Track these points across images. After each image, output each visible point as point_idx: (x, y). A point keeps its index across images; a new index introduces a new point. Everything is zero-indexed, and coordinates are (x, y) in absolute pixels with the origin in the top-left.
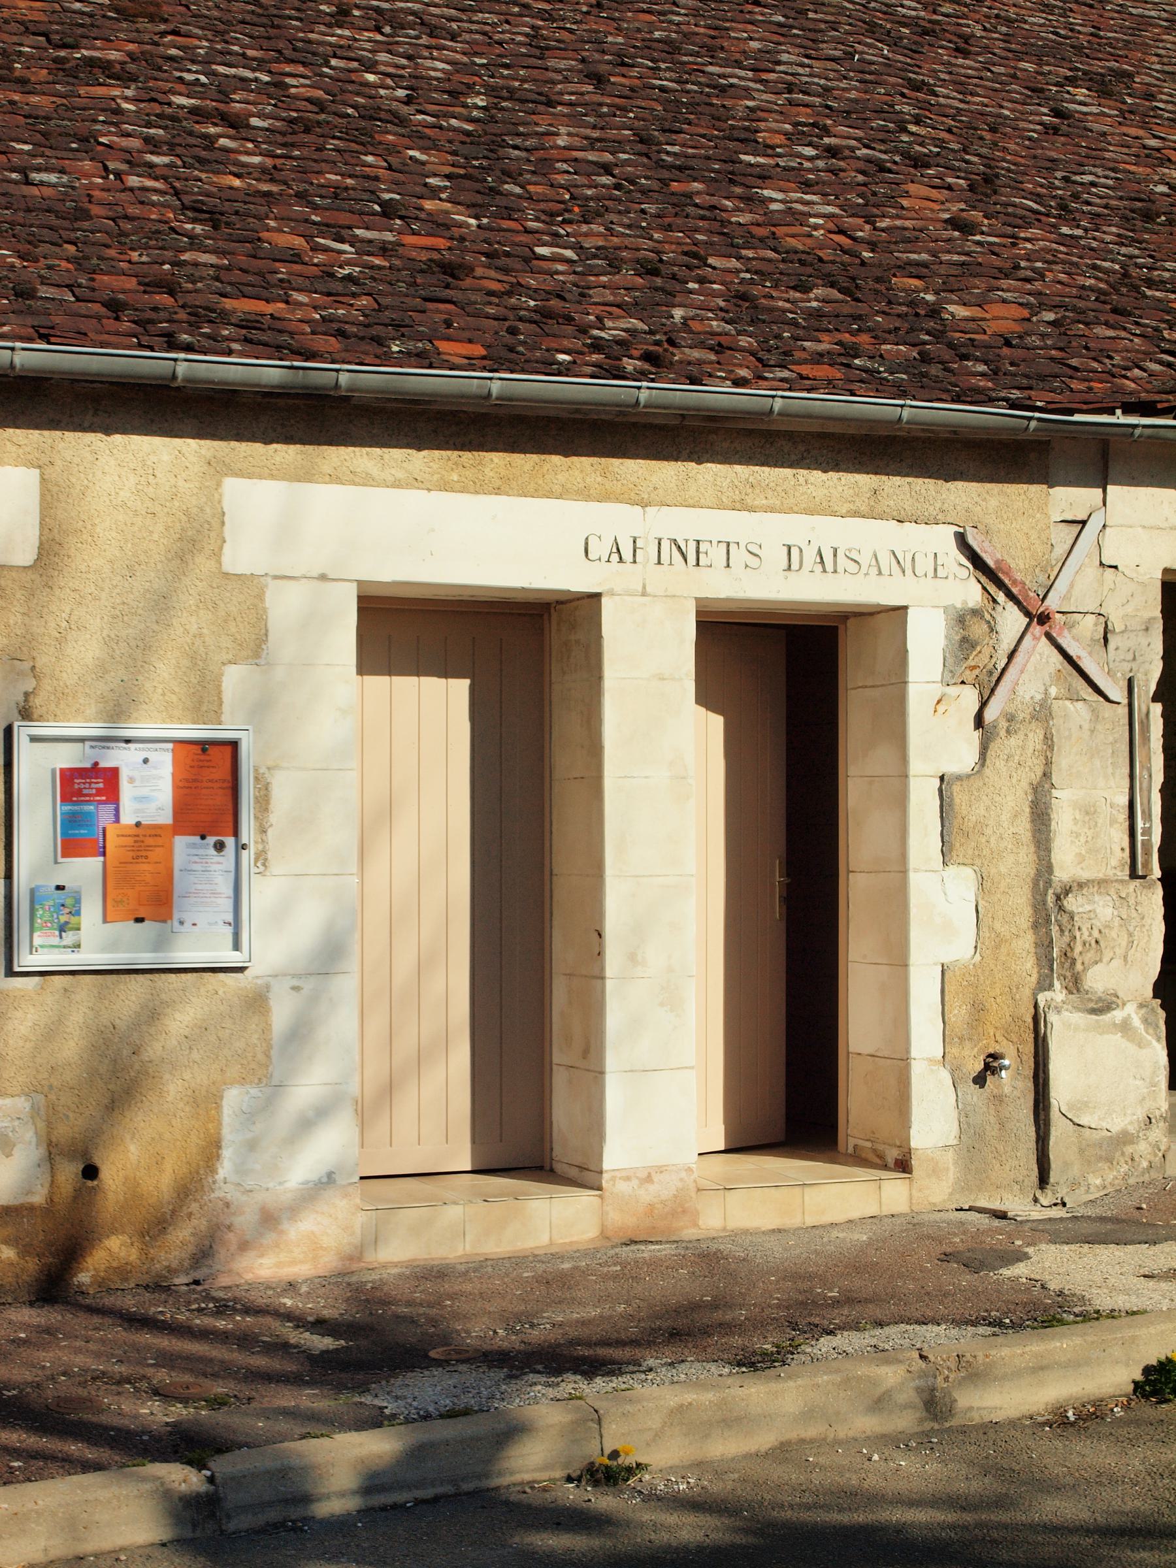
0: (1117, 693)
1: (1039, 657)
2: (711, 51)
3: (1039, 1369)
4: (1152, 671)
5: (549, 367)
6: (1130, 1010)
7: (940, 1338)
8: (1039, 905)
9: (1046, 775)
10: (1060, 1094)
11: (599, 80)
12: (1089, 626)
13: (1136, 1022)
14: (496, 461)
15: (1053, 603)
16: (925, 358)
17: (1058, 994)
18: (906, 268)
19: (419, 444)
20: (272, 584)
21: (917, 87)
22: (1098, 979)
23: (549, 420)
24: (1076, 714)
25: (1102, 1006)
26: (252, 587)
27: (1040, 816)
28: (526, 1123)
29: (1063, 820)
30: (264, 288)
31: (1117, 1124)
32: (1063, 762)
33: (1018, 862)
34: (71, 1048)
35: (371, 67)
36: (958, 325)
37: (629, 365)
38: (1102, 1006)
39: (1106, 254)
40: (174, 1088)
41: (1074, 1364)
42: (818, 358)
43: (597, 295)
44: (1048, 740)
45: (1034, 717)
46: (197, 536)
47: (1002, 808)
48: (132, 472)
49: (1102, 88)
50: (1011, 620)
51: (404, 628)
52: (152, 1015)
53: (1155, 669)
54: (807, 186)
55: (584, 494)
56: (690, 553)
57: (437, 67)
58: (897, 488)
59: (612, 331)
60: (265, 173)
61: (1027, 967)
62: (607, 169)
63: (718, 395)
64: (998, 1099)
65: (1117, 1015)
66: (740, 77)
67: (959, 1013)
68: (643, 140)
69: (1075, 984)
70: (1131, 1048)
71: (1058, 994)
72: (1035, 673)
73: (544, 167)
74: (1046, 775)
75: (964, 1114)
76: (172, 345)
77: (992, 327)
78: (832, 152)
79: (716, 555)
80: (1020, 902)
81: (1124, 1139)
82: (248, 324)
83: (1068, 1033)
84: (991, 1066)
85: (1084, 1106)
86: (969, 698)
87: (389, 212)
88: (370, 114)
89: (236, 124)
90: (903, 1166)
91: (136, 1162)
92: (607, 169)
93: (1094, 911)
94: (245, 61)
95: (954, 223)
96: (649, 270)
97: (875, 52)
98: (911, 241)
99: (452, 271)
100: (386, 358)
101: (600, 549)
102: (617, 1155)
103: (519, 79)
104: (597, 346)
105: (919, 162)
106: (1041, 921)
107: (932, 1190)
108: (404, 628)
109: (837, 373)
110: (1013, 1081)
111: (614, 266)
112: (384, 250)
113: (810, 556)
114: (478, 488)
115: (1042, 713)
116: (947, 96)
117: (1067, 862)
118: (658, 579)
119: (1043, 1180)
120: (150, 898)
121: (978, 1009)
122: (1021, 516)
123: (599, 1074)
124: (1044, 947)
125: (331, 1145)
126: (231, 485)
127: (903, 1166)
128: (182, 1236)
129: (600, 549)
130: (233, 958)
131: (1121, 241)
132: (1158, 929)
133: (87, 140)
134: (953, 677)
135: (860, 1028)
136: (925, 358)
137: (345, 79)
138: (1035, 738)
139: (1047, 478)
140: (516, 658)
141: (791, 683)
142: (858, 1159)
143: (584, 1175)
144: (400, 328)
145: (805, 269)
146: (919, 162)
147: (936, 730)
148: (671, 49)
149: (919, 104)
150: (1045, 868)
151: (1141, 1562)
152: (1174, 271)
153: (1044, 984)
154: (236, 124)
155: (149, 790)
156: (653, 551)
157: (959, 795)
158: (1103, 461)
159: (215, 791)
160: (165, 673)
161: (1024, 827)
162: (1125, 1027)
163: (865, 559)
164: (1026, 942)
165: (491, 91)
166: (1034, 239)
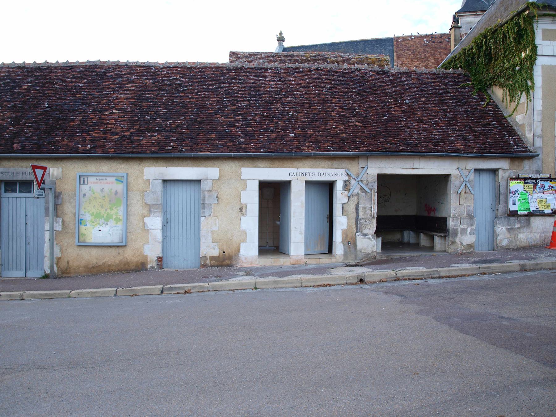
6: (370, 236)
14: (277, 163)
20: (248, 181)
23: (269, 158)
29: (360, 210)
32: (361, 201)
38: (365, 235)
44: (358, 198)
45: (356, 195)
47: (351, 208)
55: (289, 167)
56: (304, 174)
58: (335, 163)
61: (355, 230)
65: (368, 237)
69: (362, 233)
85: (361, 250)
113: (322, 174)
115: (358, 194)
117: (361, 214)
118: (299, 178)
121: (347, 236)
122: (355, 167)
124: (357, 227)
138: (356, 198)
152: (555, 213)
156: (297, 175)
161: (354, 210)
162: (369, 238)
164: (354, 226)
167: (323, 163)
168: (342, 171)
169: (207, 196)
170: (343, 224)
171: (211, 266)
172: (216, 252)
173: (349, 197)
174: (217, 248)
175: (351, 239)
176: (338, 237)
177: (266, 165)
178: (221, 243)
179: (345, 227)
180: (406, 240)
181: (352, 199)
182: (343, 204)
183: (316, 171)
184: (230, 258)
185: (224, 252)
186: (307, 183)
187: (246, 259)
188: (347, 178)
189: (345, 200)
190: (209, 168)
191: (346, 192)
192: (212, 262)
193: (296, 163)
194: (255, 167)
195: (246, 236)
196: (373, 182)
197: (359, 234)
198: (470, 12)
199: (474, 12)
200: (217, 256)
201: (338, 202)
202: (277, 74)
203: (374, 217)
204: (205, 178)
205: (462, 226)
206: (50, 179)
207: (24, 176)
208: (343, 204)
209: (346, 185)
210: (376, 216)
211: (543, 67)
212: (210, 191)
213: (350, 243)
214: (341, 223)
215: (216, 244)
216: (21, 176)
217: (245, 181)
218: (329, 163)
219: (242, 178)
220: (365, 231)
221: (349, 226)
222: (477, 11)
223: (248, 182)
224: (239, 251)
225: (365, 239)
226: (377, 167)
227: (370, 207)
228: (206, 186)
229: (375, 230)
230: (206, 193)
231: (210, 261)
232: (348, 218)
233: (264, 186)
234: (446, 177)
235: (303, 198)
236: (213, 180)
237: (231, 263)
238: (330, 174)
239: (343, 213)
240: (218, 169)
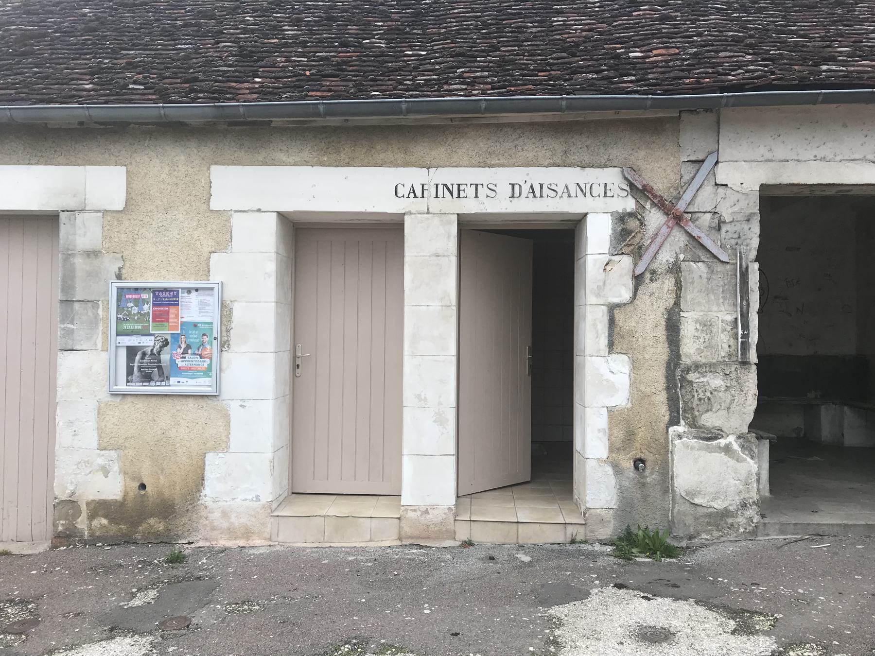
6: (731, 439)
9: (677, 304)
13: (736, 446)
27: (673, 327)
29: (688, 329)
32: (689, 296)
38: (711, 435)
44: (679, 286)
50: (655, 219)
56: (455, 191)
61: (663, 412)
65: (722, 442)
69: (693, 424)
70: (732, 462)
74: (677, 304)
80: (657, 376)
81: (725, 513)
101: (403, 191)
113: (526, 189)
117: (690, 349)
118: (436, 205)
121: (630, 436)
124: (673, 402)
129: (403, 191)
138: (669, 283)
156: (433, 196)
157: (619, 315)
161: (661, 333)
162: (727, 449)
163: (560, 189)
164: (662, 397)
167: (531, 147)
168: (612, 176)
169: (79, 274)
170: (612, 388)
171: (93, 541)
172: (112, 488)
173: (638, 280)
174: (116, 468)
175: (649, 447)
176: (592, 438)
177: (306, 155)
178: (131, 453)
179: (621, 399)
180: (827, 432)
181: (649, 287)
182: (612, 308)
183: (503, 177)
184: (166, 509)
185: (143, 486)
186: (610, 353)
187: (225, 515)
188: (630, 204)
189: (624, 294)
190: (90, 168)
191: (626, 261)
192: (95, 523)
193: (421, 150)
194: (266, 164)
195: (228, 424)
196: (739, 217)
197: (681, 428)
200: (115, 502)
201: (591, 299)
203: (745, 363)
204: (71, 204)
208: (612, 308)
209: (626, 235)
210: (753, 356)
212: (92, 254)
213: (645, 465)
214: (606, 384)
215: (113, 454)
217: (224, 216)
218: (557, 145)
219: (214, 205)
220: (709, 420)
223: (237, 221)
224: (200, 481)
225: (710, 450)
226: (743, 170)
227: (718, 322)
228: (84, 234)
229: (750, 418)
230: (78, 261)
231: (92, 517)
232: (635, 365)
233: (776, 203)
235: (449, 283)
236: (105, 212)
237: (168, 530)
238: (560, 189)
239: (611, 345)
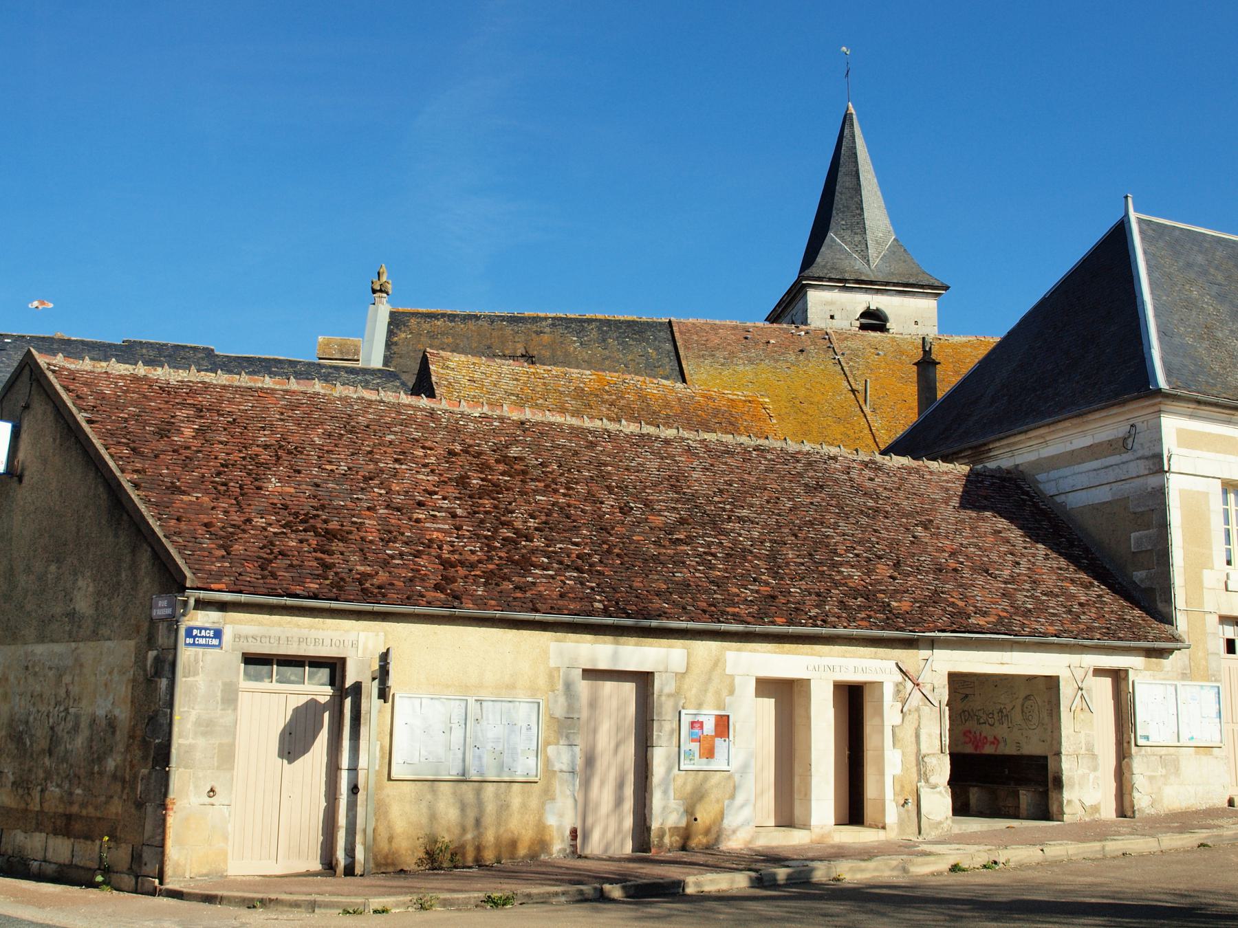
0: (937, 704)
1: (917, 695)
2: (822, 523)
3: (927, 864)
4: (945, 698)
5: (801, 625)
7: (904, 857)
8: (918, 760)
10: (923, 811)
11: (796, 536)
12: (929, 687)
15: (920, 681)
16: (888, 618)
17: (923, 783)
18: (881, 591)
19: (769, 642)
21: (875, 531)
22: (933, 780)
24: (926, 709)
25: (934, 787)
26: (732, 677)
27: (917, 736)
28: (788, 813)
29: (923, 738)
30: (734, 605)
31: (938, 819)
33: (912, 749)
34: (689, 788)
35: (740, 535)
36: (895, 608)
37: (819, 623)
38: (934, 787)
39: (930, 584)
40: (712, 797)
41: (934, 863)
42: (863, 619)
43: (808, 603)
46: (717, 663)
47: (908, 734)
48: (705, 649)
49: (926, 528)
50: (909, 685)
51: (766, 686)
52: (706, 779)
53: (947, 698)
54: (852, 567)
55: (807, 654)
57: (756, 534)
59: (813, 613)
60: (726, 570)
61: (915, 776)
62: (803, 564)
63: (840, 631)
64: (908, 811)
66: (830, 532)
67: (898, 788)
68: (811, 555)
69: (927, 781)
71: (923, 783)
72: (916, 697)
73: (787, 564)
75: (899, 815)
76: (719, 622)
77: (904, 608)
78: (857, 555)
79: (837, 669)
81: (940, 823)
82: (733, 615)
83: (925, 793)
84: (906, 802)
86: (899, 705)
87: (755, 580)
88: (744, 550)
89: (714, 555)
90: (884, 828)
91: (704, 815)
92: (803, 564)
93: (932, 762)
94: (711, 536)
95: (891, 577)
96: (818, 595)
97: (864, 520)
98: (880, 582)
99: (774, 597)
100: (764, 624)
102: (814, 822)
103: (774, 536)
104: (810, 618)
105: (880, 558)
106: (918, 764)
107: (891, 834)
108: (766, 686)
109: (867, 624)
110: (911, 806)
111: (810, 594)
112: (757, 592)
114: (783, 653)
115: (918, 709)
116: (884, 534)
117: (924, 750)
119: (920, 833)
120: (709, 753)
121: (902, 787)
122: (912, 658)
123: (810, 800)
124: (919, 770)
125: (746, 813)
126: (728, 653)
127: (884, 828)
128: (713, 836)
130: (727, 768)
131: (935, 579)
132: (949, 767)
133: (684, 563)
134: (895, 700)
135: (870, 791)
136: (888, 618)
137: (735, 539)
138: (916, 716)
139: (917, 648)
140: (786, 694)
141: (853, 700)
142: (870, 826)
143: (806, 826)
144: (767, 615)
145: (855, 593)
146: (880, 558)
147: (891, 713)
148: (811, 523)
149: (878, 538)
150: (919, 750)
151: (965, 334)
153: (919, 781)
154: (714, 555)
155: (709, 727)
156: (823, 668)
157: (897, 730)
158: (932, 644)
159: (723, 725)
160: (710, 697)
161: (913, 739)
162: (940, 793)
164: (914, 769)
165: (771, 541)
166: (912, 581)
198: (830, 280)
199: (839, 281)
202: (689, 449)
205: (1080, 772)
206: (360, 653)
207: (303, 645)
211: (1182, 493)
216: (295, 645)
221: (905, 769)
222: (846, 281)
227: (934, 733)
234: (1052, 683)
240: (1156, 791)
